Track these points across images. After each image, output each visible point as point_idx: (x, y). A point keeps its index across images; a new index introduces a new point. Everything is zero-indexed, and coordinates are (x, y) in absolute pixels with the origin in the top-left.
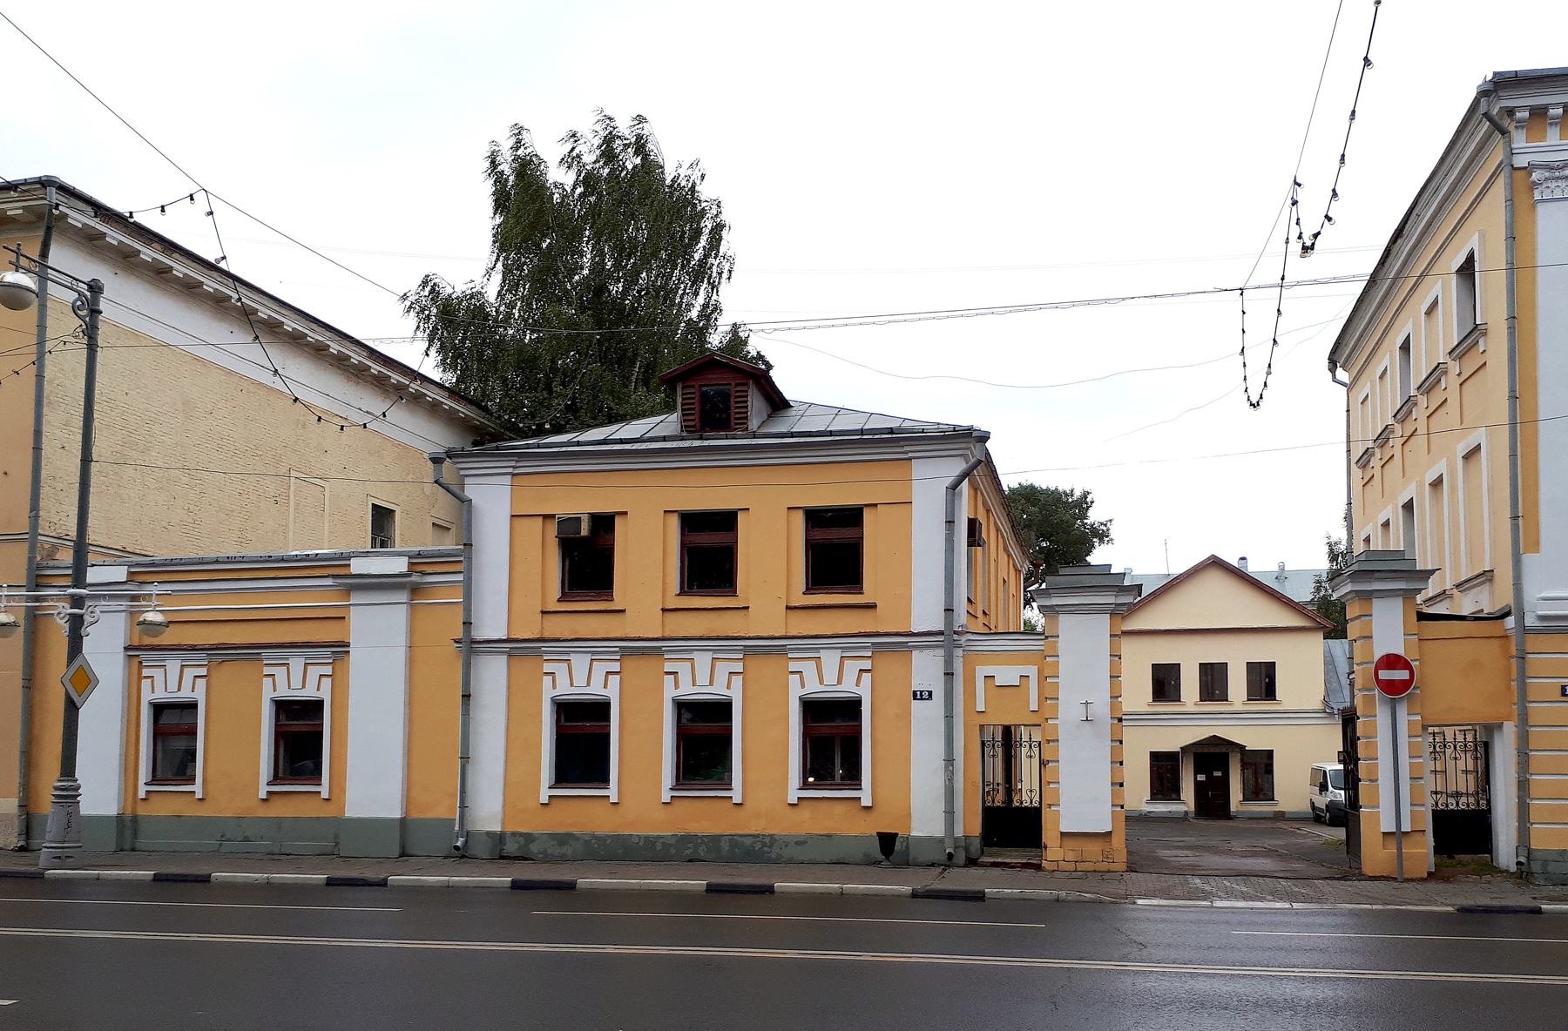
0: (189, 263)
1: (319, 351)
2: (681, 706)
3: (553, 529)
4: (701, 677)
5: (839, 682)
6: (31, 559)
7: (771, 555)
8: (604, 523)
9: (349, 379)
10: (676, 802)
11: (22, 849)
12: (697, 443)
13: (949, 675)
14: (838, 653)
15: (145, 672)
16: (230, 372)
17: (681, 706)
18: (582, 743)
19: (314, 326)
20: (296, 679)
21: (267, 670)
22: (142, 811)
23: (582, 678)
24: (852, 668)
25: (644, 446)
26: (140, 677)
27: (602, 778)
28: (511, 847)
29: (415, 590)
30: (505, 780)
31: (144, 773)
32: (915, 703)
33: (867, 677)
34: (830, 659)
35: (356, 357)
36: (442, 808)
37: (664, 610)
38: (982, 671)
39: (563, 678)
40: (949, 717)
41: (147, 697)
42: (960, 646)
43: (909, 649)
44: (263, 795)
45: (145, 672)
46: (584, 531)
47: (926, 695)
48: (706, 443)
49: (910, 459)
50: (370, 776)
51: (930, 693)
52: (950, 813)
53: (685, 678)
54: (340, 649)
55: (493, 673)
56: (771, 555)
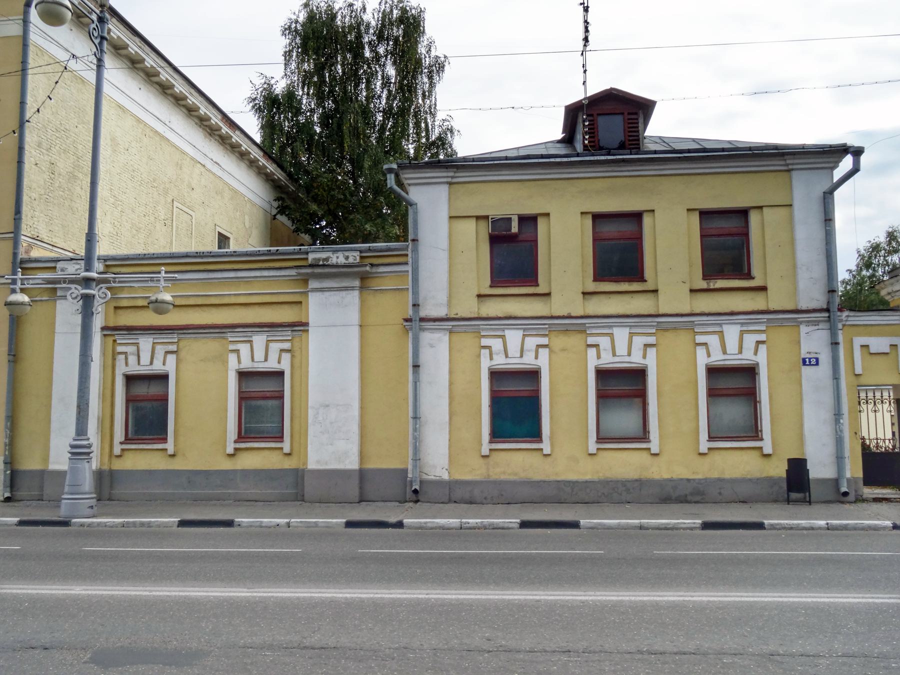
0: (121, 27)
1: (190, 111)
2: (496, 375)
3: (485, 230)
4: (621, 348)
5: (740, 352)
6: (15, 255)
7: (672, 246)
8: (529, 221)
9: (206, 137)
10: (601, 452)
11: (8, 500)
12: (592, 158)
13: (835, 344)
14: (627, 330)
15: (120, 349)
16: (139, 120)
17: (496, 375)
18: (516, 407)
19: (193, 91)
20: (259, 353)
21: (232, 347)
22: (118, 465)
23: (515, 349)
24: (750, 340)
25: (552, 160)
26: (115, 354)
27: (536, 434)
28: (458, 493)
29: (364, 278)
30: (448, 439)
31: (119, 434)
32: (804, 368)
33: (652, 352)
34: (732, 332)
35: (216, 119)
36: (384, 460)
37: (584, 293)
38: (858, 341)
39: (132, 359)
40: (836, 377)
41: (121, 369)
42: (841, 321)
43: (798, 324)
44: (230, 450)
45: (120, 349)
46: (515, 229)
47: (813, 361)
48: (596, 158)
49: (792, 170)
50: (329, 438)
51: (817, 359)
52: (839, 459)
53: (132, 359)
54: (300, 326)
55: (436, 348)
56: (672, 246)
